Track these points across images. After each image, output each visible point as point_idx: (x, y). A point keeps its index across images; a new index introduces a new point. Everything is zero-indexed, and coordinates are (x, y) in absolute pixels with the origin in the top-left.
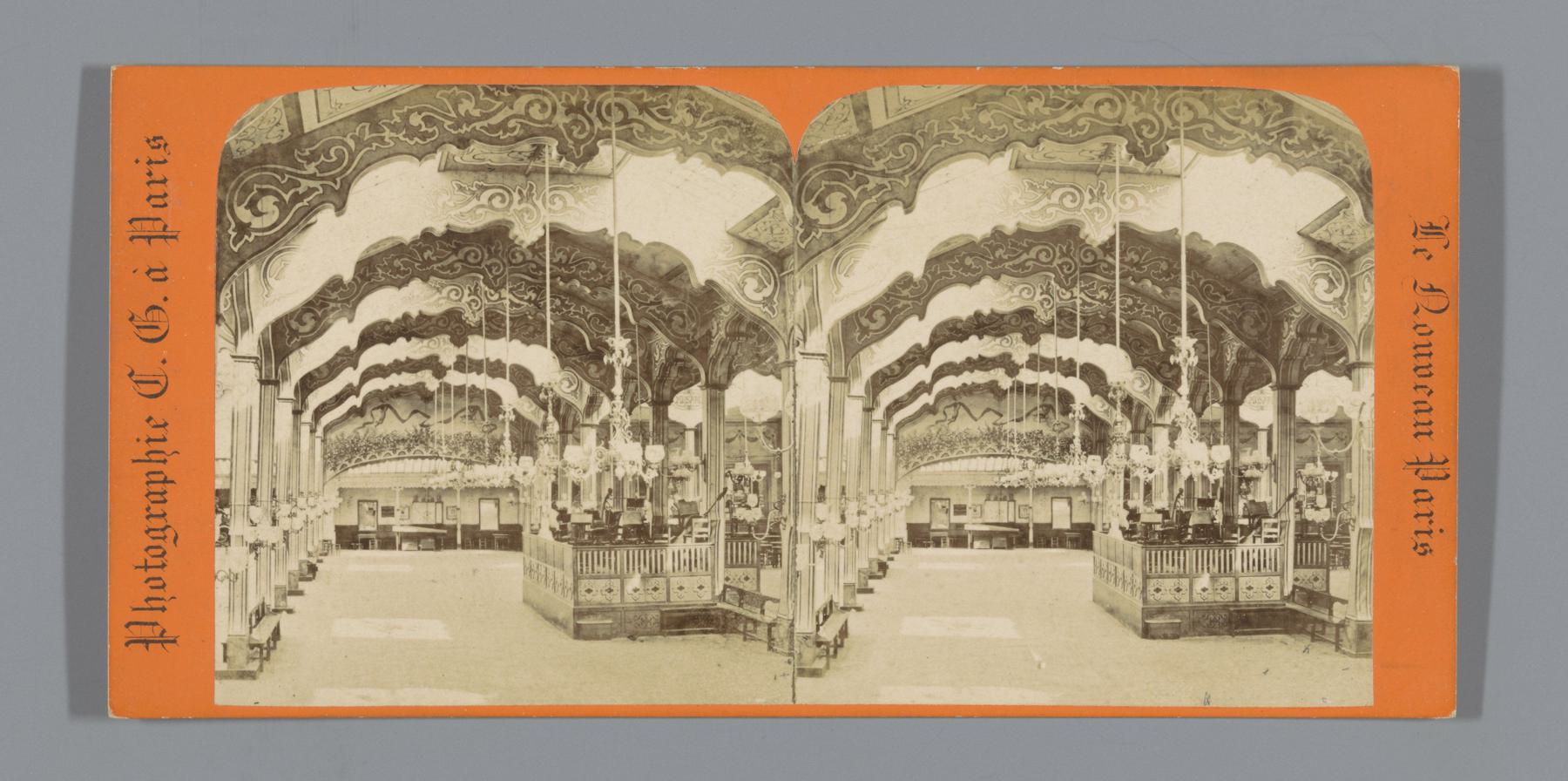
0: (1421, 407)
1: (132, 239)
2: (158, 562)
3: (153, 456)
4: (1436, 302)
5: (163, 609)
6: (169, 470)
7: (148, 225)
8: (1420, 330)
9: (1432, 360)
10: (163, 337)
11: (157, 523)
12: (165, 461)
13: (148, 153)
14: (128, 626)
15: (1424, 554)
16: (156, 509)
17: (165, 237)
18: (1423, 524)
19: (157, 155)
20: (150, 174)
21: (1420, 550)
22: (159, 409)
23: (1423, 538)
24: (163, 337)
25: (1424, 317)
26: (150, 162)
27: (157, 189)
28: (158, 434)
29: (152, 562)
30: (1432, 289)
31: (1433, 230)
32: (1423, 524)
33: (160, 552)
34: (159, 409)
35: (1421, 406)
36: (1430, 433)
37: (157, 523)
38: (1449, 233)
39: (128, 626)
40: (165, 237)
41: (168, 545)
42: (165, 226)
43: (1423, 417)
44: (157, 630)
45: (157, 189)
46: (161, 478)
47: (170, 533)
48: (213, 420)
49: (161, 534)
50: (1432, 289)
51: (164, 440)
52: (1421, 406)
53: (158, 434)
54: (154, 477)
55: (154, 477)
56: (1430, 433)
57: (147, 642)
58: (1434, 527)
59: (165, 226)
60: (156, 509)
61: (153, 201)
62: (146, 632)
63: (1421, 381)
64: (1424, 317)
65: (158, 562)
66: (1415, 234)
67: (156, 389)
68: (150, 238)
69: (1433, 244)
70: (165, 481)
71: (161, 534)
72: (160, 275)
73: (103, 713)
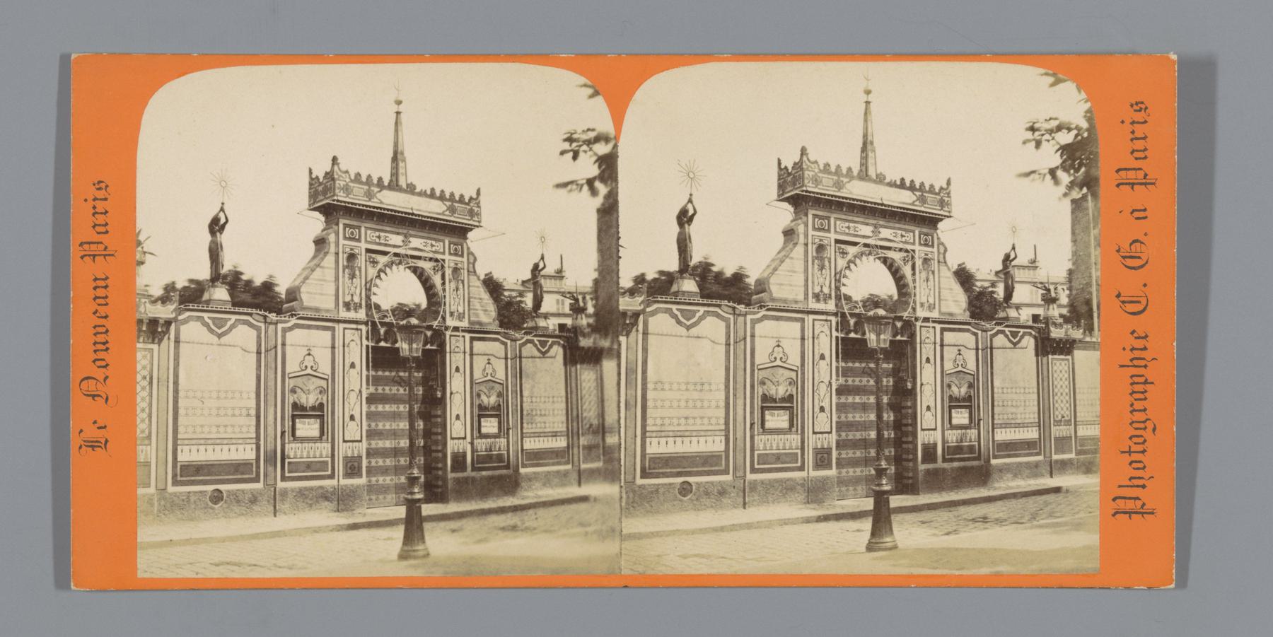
0: (101, 300)
1: (1118, 186)
2: (1140, 448)
3: (1135, 362)
4: (91, 386)
5: (1144, 486)
6: (1149, 374)
7: (1131, 174)
8: (103, 363)
9: (94, 339)
10: (1142, 266)
11: (1139, 416)
12: (1145, 366)
13: (1131, 115)
14: (1114, 500)
15: (100, 182)
16: (1138, 405)
17: (1145, 184)
18: (100, 206)
19: (1140, 117)
20: (1133, 132)
21: (103, 185)
22: (1139, 323)
23: (101, 194)
24: (1142, 266)
25: (100, 374)
26: (1133, 123)
27: (1139, 145)
28: (1139, 343)
29: (1134, 448)
30: (94, 396)
31: (93, 445)
32: (100, 206)
33: (1141, 440)
34: (1139, 323)
35: (102, 301)
36: (95, 279)
37: (1139, 416)
38: (80, 442)
39: (1114, 500)
40: (1145, 184)
41: (1148, 434)
42: (1146, 175)
43: (101, 292)
44: (1139, 503)
45: (1139, 145)
46: (1142, 380)
47: (1150, 425)
48: (135, 197)
49: (1142, 425)
50: (94, 396)
51: (1145, 348)
52: (102, 301)
53: (1139, 343)
54: (1136, 379)
55: (1136, 379)
56: (95, 279)
57: (1130, 513)
58: (91, 204)
59: (1146, 175)
60: (1138, 405)
61: (1136, 154)
62: (1130, 505)
63: (103, 322)
64: (100, 374)
65: (1140, 448)
66: (107, 441)
67: (1140, 307)
68: (1133, 184)
69: (91, 433)
70: (1146, 382)
71: (1142, 425)
72: (1141, 214)
73: (1182, 62)
